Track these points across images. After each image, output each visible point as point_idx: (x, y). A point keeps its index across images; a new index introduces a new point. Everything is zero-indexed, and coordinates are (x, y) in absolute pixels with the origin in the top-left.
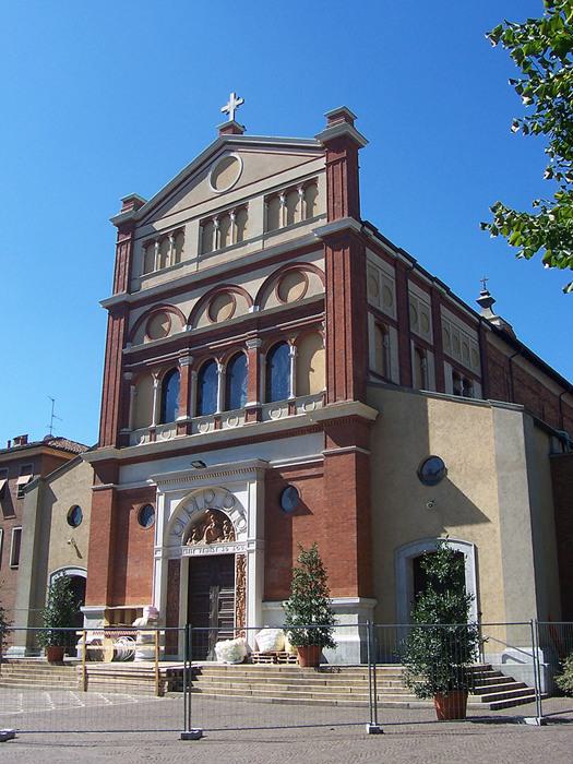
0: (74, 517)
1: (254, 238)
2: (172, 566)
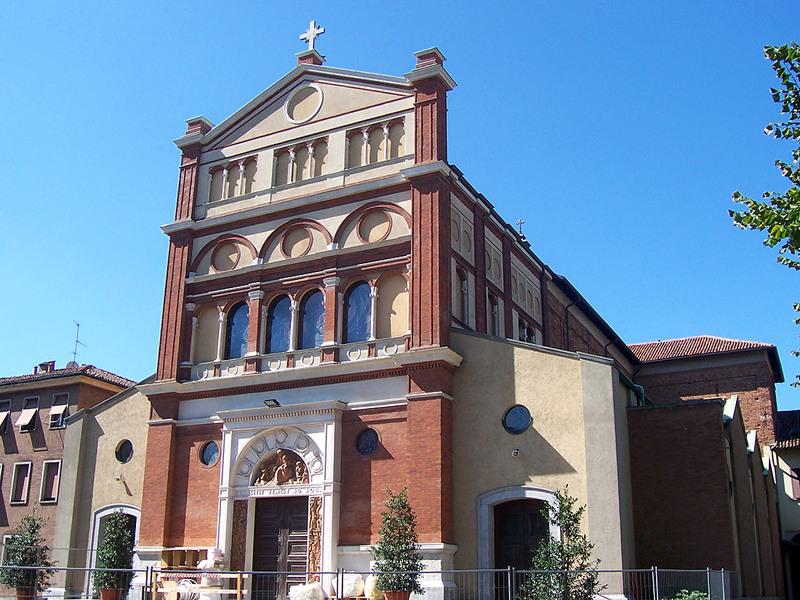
0: (124, 451)
1: (333, 172)
2: (239, 507)
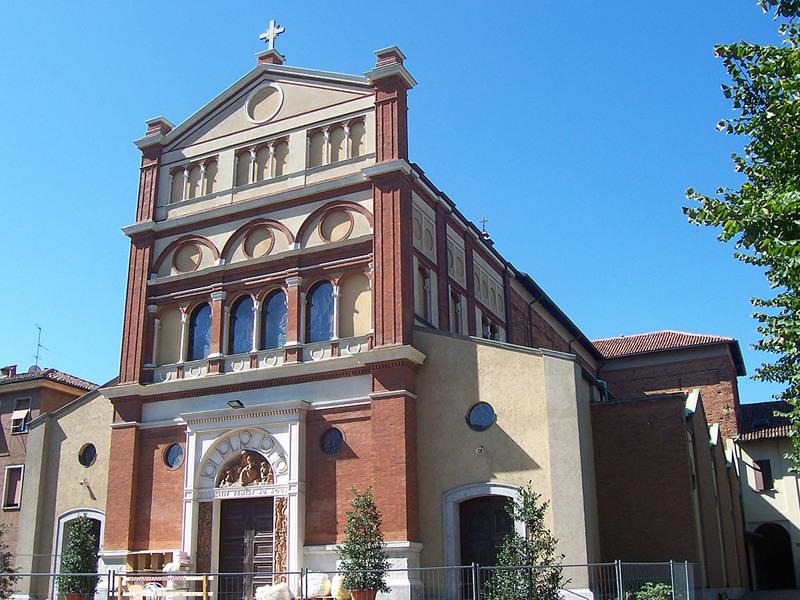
0: (87, 455)
1: (295, 172)
2: (203, 509)
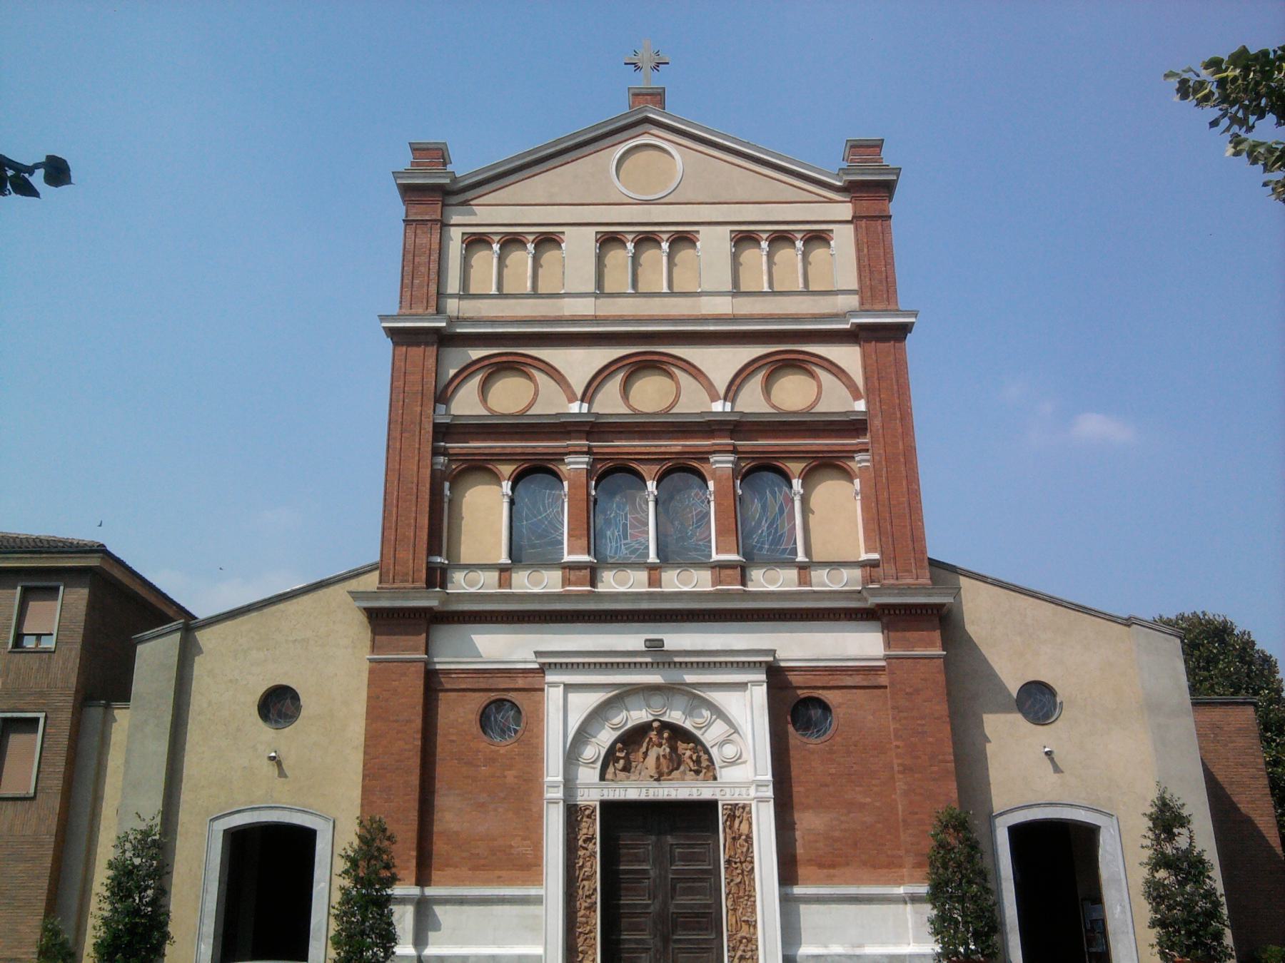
2: (573, 814)
